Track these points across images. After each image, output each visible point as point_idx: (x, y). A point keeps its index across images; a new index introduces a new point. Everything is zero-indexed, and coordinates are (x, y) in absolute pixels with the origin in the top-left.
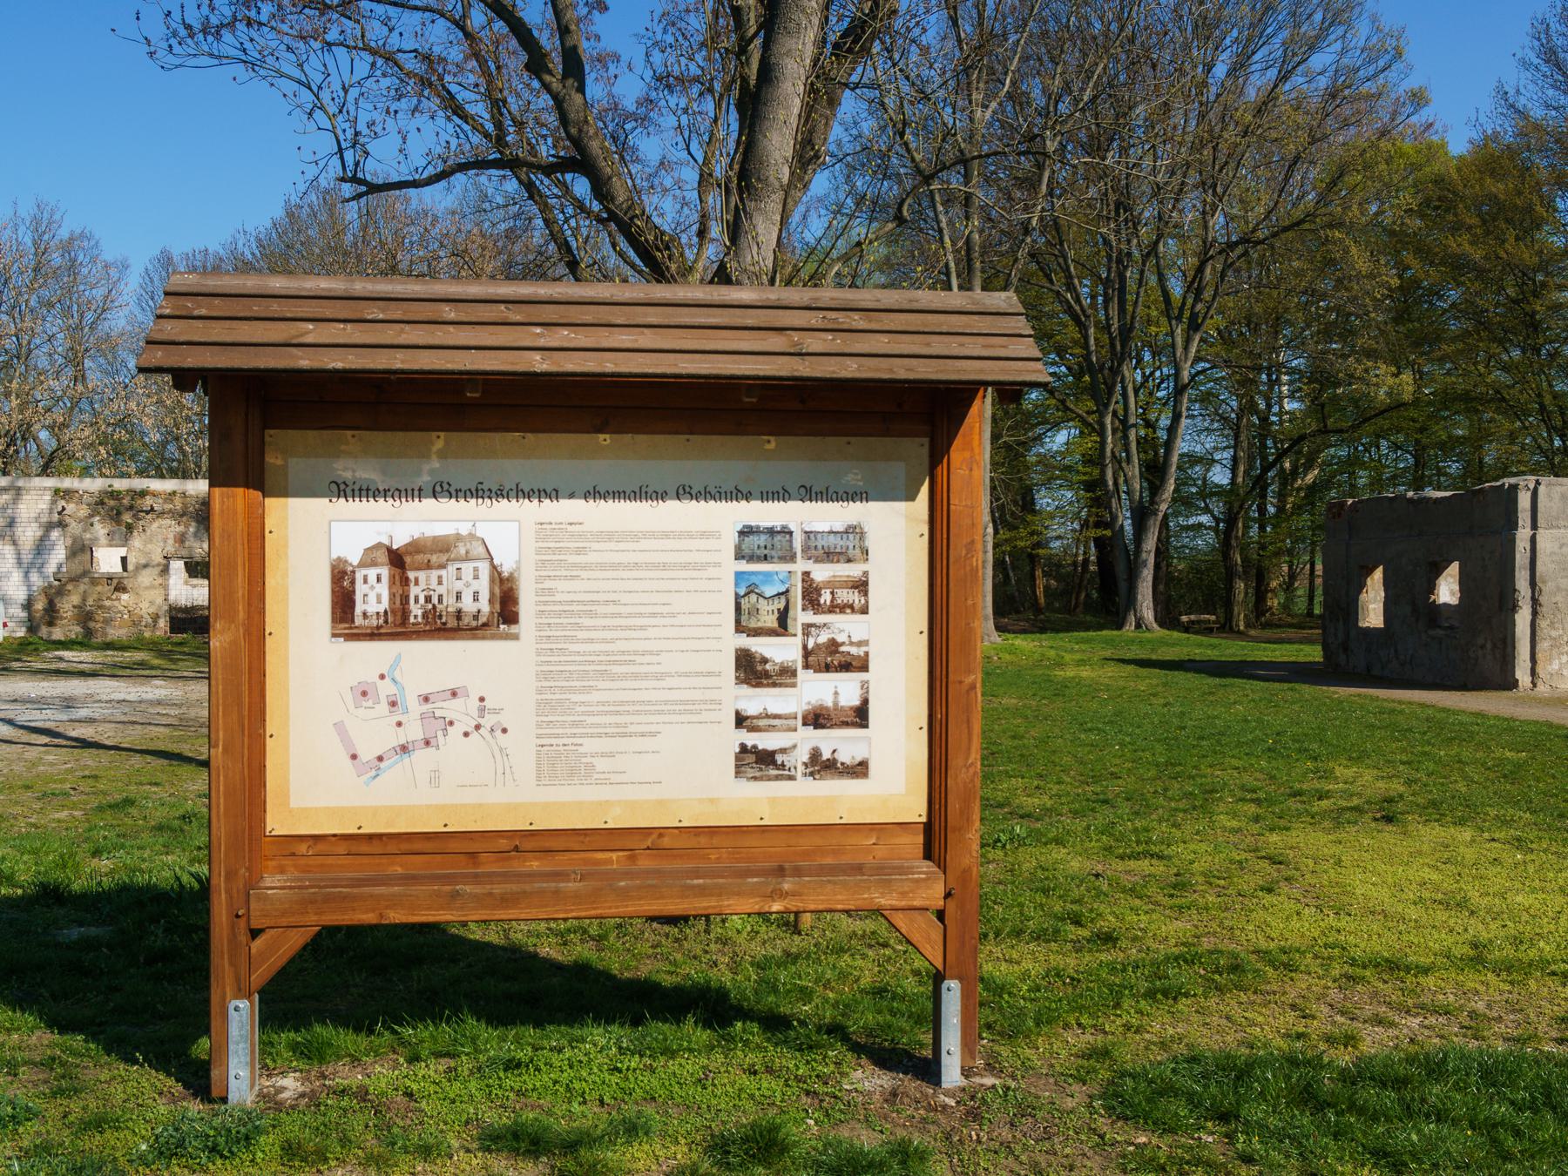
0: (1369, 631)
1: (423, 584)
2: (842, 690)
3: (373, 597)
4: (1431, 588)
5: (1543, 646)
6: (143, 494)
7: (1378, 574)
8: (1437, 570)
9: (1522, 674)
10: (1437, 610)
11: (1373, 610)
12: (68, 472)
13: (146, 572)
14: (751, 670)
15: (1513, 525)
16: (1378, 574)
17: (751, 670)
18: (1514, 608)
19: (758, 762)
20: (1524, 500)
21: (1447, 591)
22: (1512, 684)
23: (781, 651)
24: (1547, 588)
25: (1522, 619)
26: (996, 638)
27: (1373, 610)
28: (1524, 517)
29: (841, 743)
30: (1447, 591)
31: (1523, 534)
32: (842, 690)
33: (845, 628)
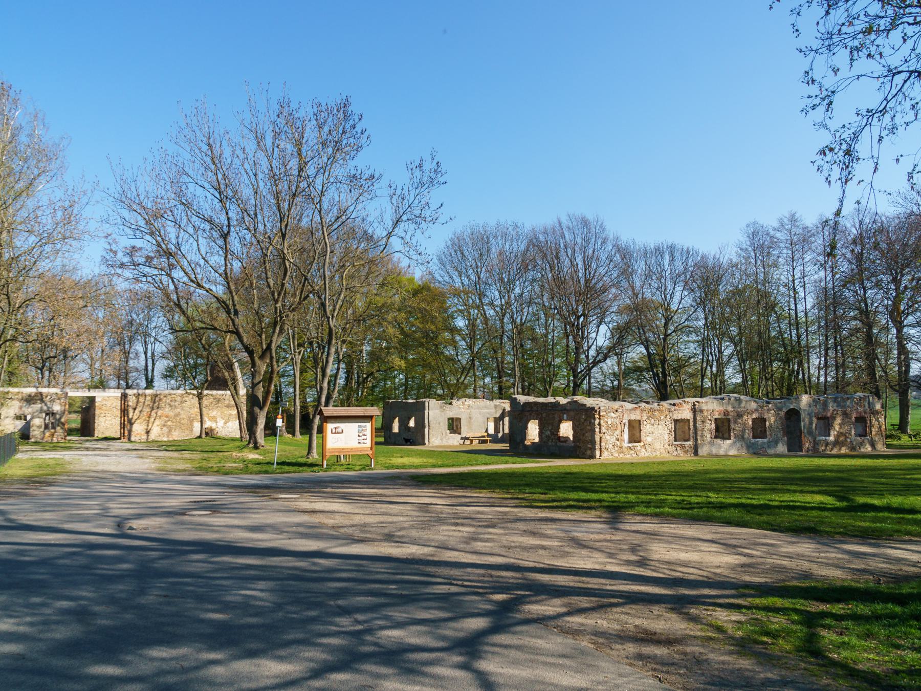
0: (395, 433)
1: (337, 430)
2: (365, 437)
3: (334, 431)
4: (409, 423)
5: (431, 435)
6: (8, 393)
7: (397, 419)
8: (410, 419)
9: (427, 442)
10: (409, 428)
11: (396, 428)
12: (20, 387)
13: (8, 419)
14: (359, 436)
15: (424, 409)
16: (397, 419)
17: (359, 436)
18: (425, 427)
19: (359, 443)
20: (427, 404)
21: (412, 423)
22: (424, 444)
23: (361, 434)
24: (431, 423)
25: (426, 430)
26: (300, 437)
27: (396, 428)
28: (427, 408)
29: (365, 441)
30: (412, 423)
31: (426, 411)
32: (365, 437)
33: (365, 433)
